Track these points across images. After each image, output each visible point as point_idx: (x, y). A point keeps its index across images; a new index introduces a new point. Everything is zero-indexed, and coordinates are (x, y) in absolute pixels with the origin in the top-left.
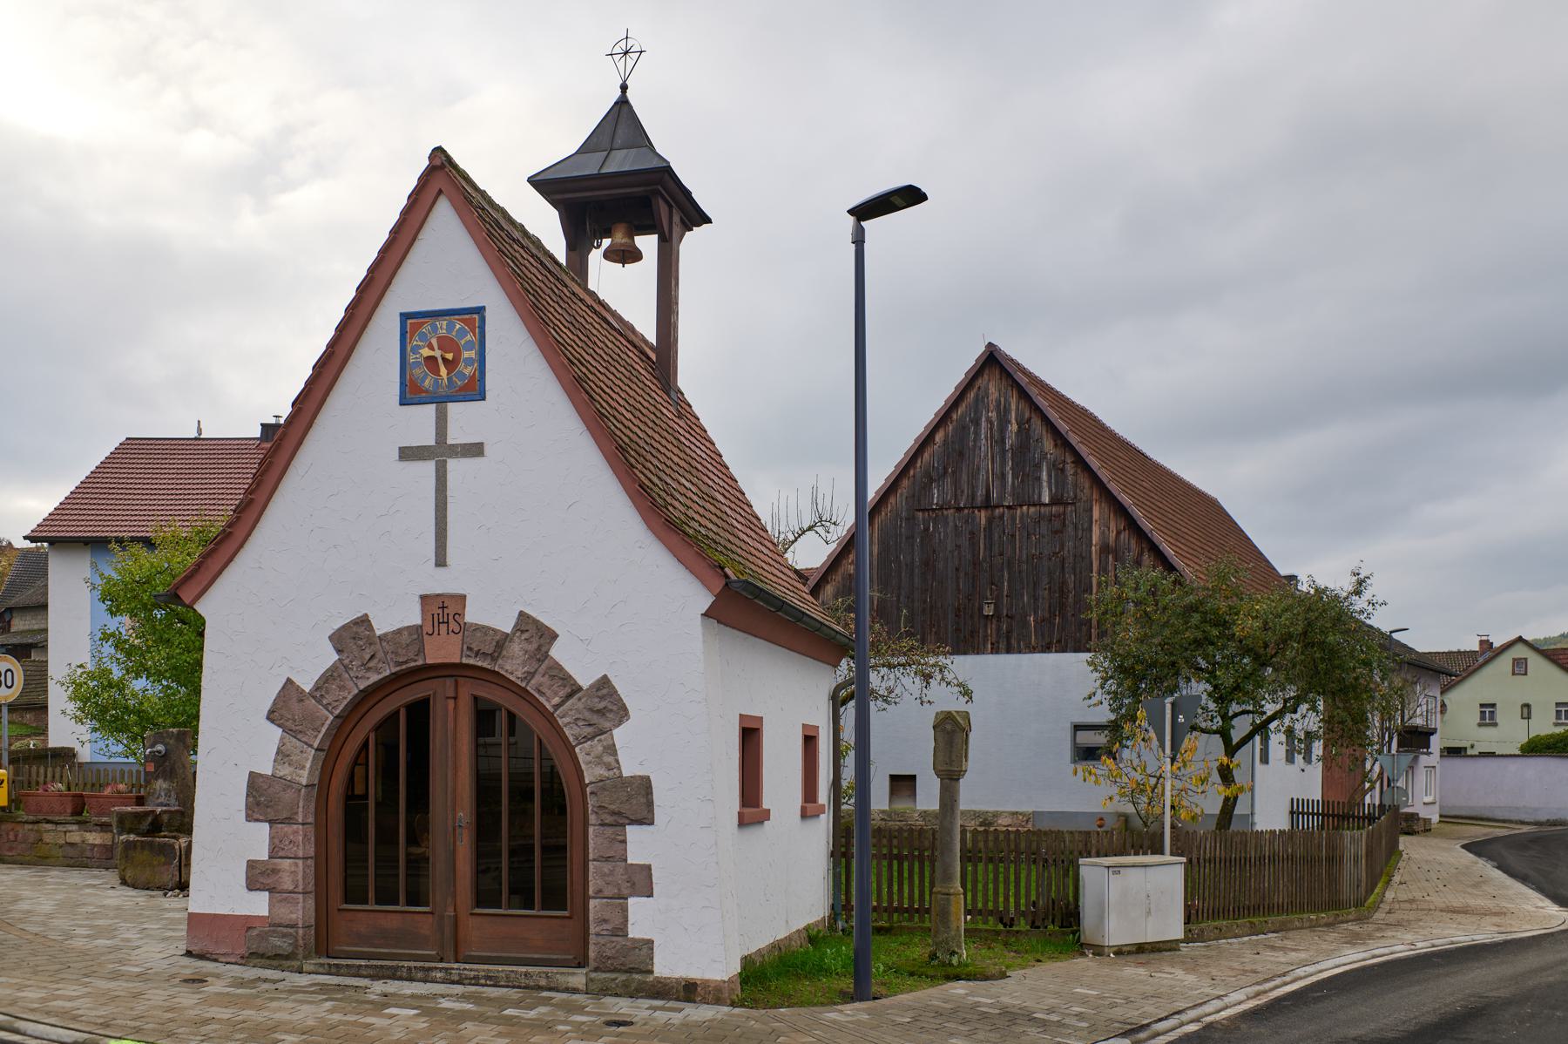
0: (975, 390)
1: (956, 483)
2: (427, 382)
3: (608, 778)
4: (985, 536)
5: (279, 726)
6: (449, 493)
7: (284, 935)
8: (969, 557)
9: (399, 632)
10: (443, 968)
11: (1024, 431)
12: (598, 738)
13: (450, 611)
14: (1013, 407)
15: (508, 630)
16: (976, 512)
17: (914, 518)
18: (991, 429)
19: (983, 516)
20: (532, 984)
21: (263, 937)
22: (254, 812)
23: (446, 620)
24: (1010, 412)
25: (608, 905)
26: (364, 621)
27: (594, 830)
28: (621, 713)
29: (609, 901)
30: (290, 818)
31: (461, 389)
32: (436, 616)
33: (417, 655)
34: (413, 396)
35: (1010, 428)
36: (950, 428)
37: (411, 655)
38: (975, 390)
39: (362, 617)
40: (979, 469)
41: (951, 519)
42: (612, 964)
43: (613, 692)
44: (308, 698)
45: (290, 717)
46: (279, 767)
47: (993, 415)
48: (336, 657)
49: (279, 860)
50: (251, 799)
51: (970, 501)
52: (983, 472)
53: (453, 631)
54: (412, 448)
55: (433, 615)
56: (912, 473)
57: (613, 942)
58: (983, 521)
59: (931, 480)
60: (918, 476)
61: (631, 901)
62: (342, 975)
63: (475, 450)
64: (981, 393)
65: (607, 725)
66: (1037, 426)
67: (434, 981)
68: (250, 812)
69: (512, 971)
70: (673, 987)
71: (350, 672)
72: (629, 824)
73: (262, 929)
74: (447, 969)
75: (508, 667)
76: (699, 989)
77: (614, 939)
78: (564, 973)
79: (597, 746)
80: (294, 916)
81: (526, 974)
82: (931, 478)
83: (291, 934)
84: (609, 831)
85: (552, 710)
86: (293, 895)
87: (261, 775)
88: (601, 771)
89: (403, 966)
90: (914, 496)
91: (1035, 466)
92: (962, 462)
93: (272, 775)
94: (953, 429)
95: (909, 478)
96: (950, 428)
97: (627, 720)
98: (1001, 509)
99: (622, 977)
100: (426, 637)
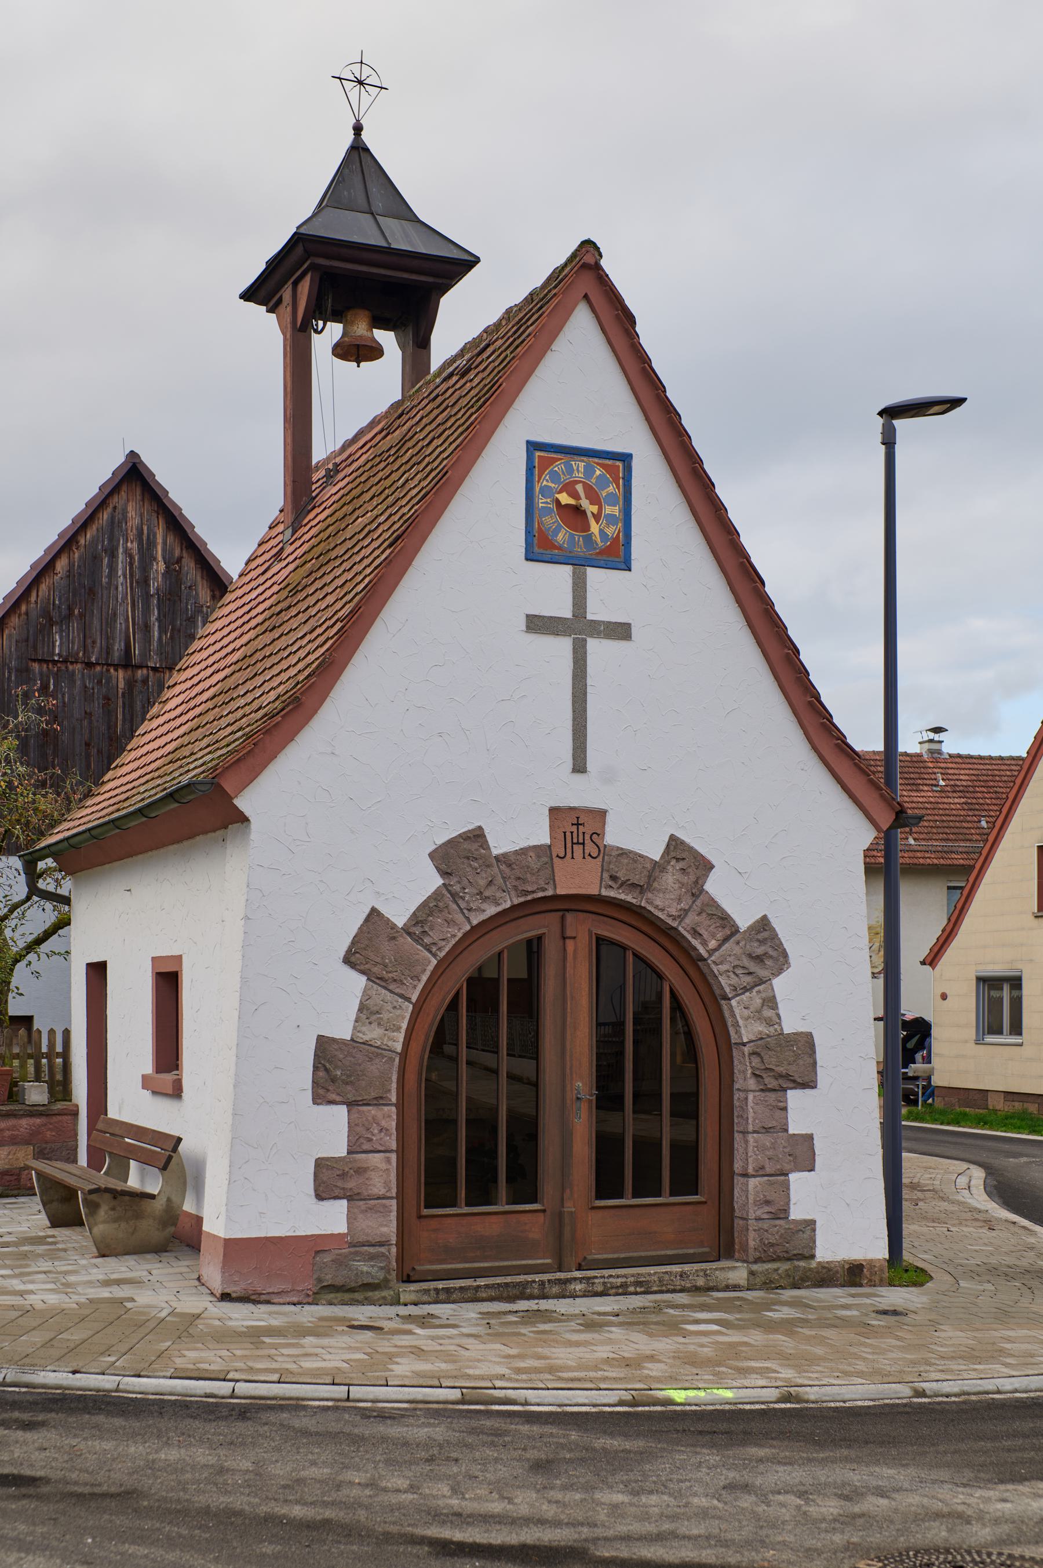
0: (110, 510)
1: (85, 630)
2: (560, 536)
3: (769, 1036)
4: (124, 703)
5: (363, 972)
6: (589, 682)
7: (372, 1257)
8: (103, 728)
9: (524, 851)
10: (583, 1278)
11: (173, 573)
12: (757, 989)
13: (588, 829)
14: (160, 540)
15: (656, 856)
16: (112, 670)
17: (28, 670)
18: (131, 564)
19: (120, 677)
20: (688, 1285)
21: (340, 1262)
22: (328, 1090)
23: (581, 841)
24: (155, 546)
25: (771, 1184)
26: (477, 836)
27: (755, 1097)
28: (781, 960)
29: (770, 1178)
30: (381, 1098)
31: (602, 552)
32: (568, 835)
33: (547, 884)
34: (541, 551)
35: (155, 567)
36: (76, 555)
37: (542, 884)
38: (110, 510)
39: (473, 830)
40: (115, 614)
41: (78, 676)
42: (775, 1252)
43: (774, 936)
44: (401, 936)
45: (378, 960)
46: (364, 1029)
47: (133, 546)
48: (439, 881)
49: (363, 1155)
50: (321, 1074)
51: (104, 656)
52: (120, 620)
53: (590, 855)
54: (544, 617)
55: (565, 833)
56: (24, 608)
57: (776, 1226)
58: (121, 684)
59: (51, 623)
60: (33, 615)
61: (793, 1177)
62: (454, 1302)
63: (621, 631)
64: (118, 516)
65: (763, 973)
66: (190, 568)
67: (574, 1296)
68: (321, 1092)
69: (666, 1273)
70: (837, 1272)
71: (460, 902)
72: (791, 1089)
73: (337, 1252)
74: (589, 1278)
75: (658, 902)
76: (865, 1270)
77: (778, 1222)
78: (723, 1268)
79: (754, 998)
80: (384, 1229)
81: (682, 1275)
82: (51, 619)
83: (383, 1255)
84: (772, 1096)
85: (705, 954)
86: (384, 1201)
87: (334, 1040)
88: (760, 1028)
89: (534, 1281)
90: (27, 640)
91: (188, 619)
92: (93, 603)
93: (352, 1040)
94: (80, 558)
95: (20, 615)
96: (76, 555)
97: (787, 968)
98: (145, 671)
99: (783, 1266)
100: (556, 860)
